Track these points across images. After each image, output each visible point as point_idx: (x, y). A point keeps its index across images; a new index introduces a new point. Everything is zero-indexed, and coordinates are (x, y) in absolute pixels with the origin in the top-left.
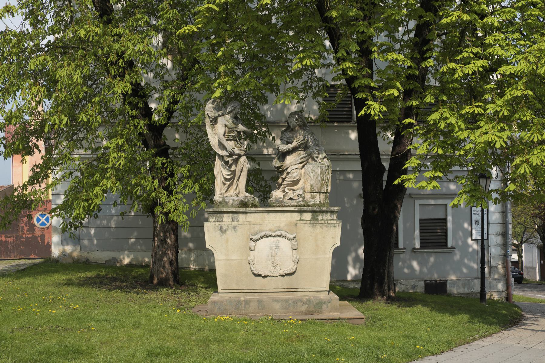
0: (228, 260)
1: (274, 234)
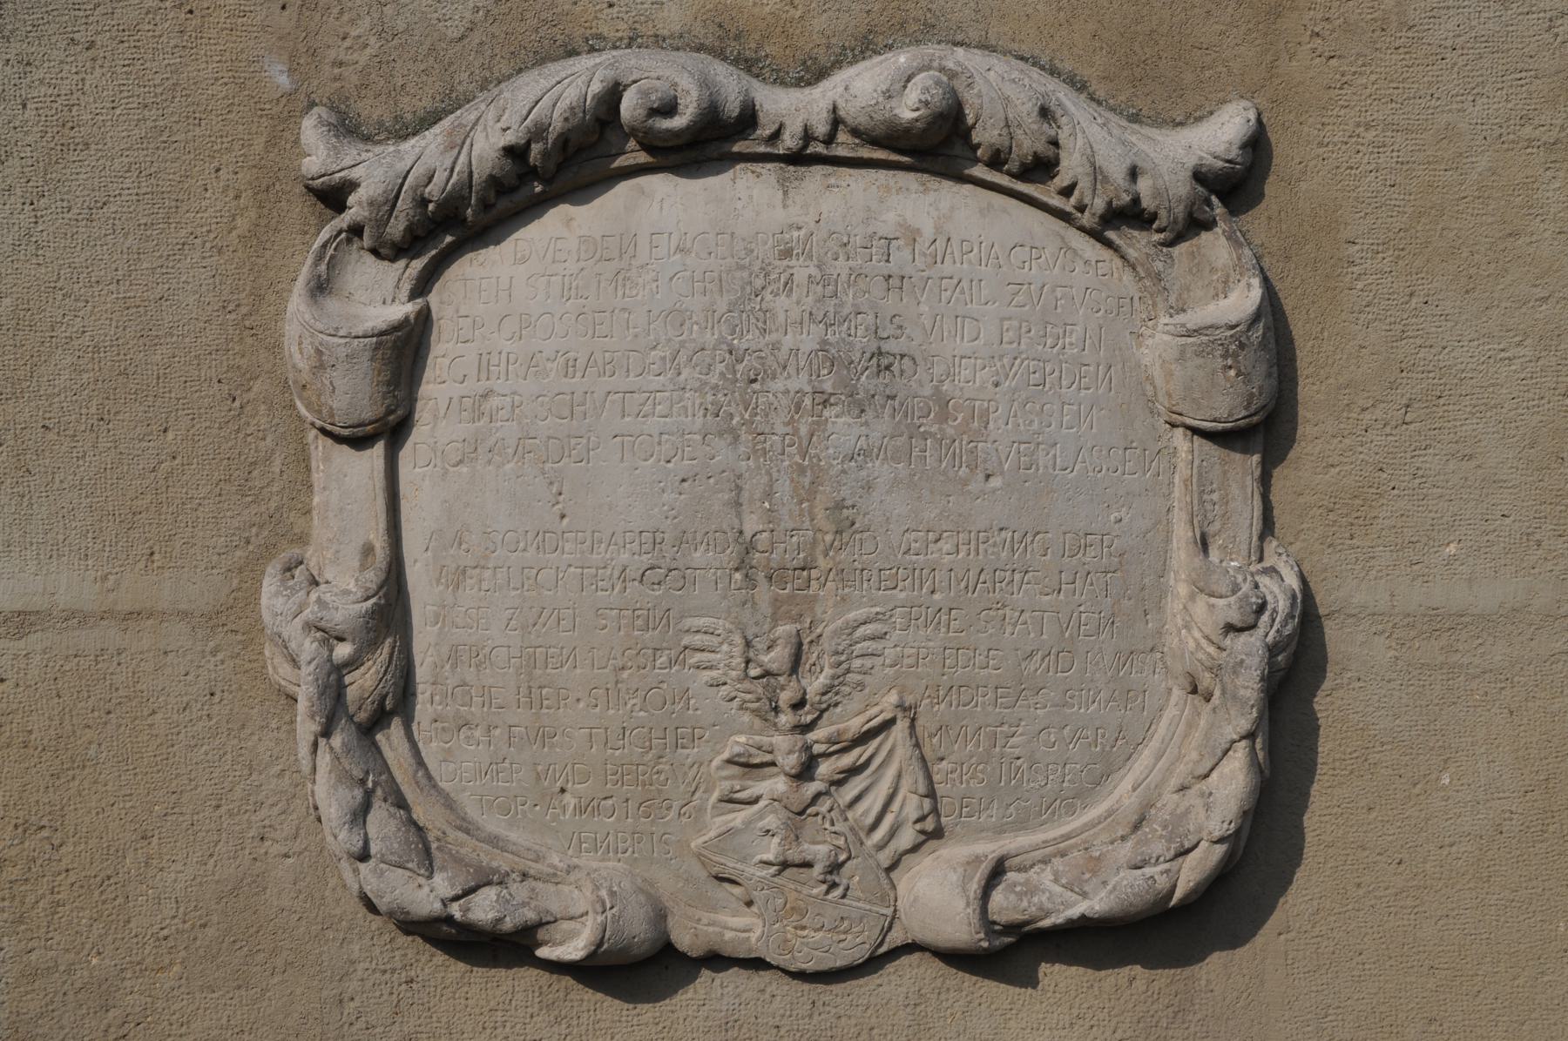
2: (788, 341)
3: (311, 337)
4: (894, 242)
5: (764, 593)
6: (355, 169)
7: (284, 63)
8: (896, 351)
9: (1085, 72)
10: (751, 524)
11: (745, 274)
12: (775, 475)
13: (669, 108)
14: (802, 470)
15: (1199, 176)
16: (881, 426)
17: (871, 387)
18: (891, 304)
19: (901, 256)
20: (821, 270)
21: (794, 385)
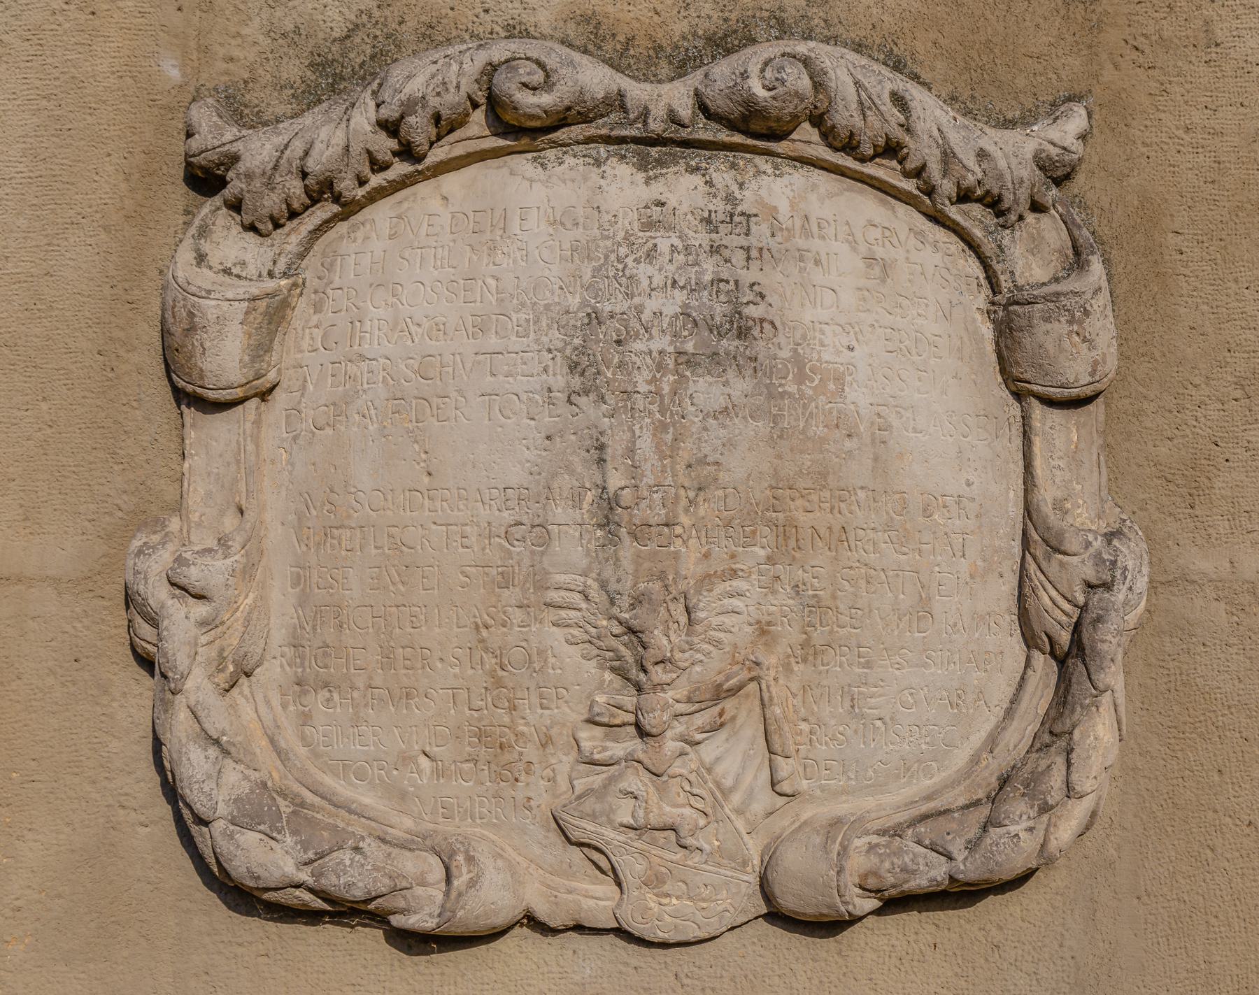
2: (651, 305)
3: (184, 300)
4: (753, 219)
5: (628, 549)
6: (235, 144)
7: (176, 58)
8: (755, 315)
10: (616, 481)
11: (609, 243)
12: (638, 433)
14: (663, 427)
17: (731, 348)
20: (682, 241)
21: (655, 346)
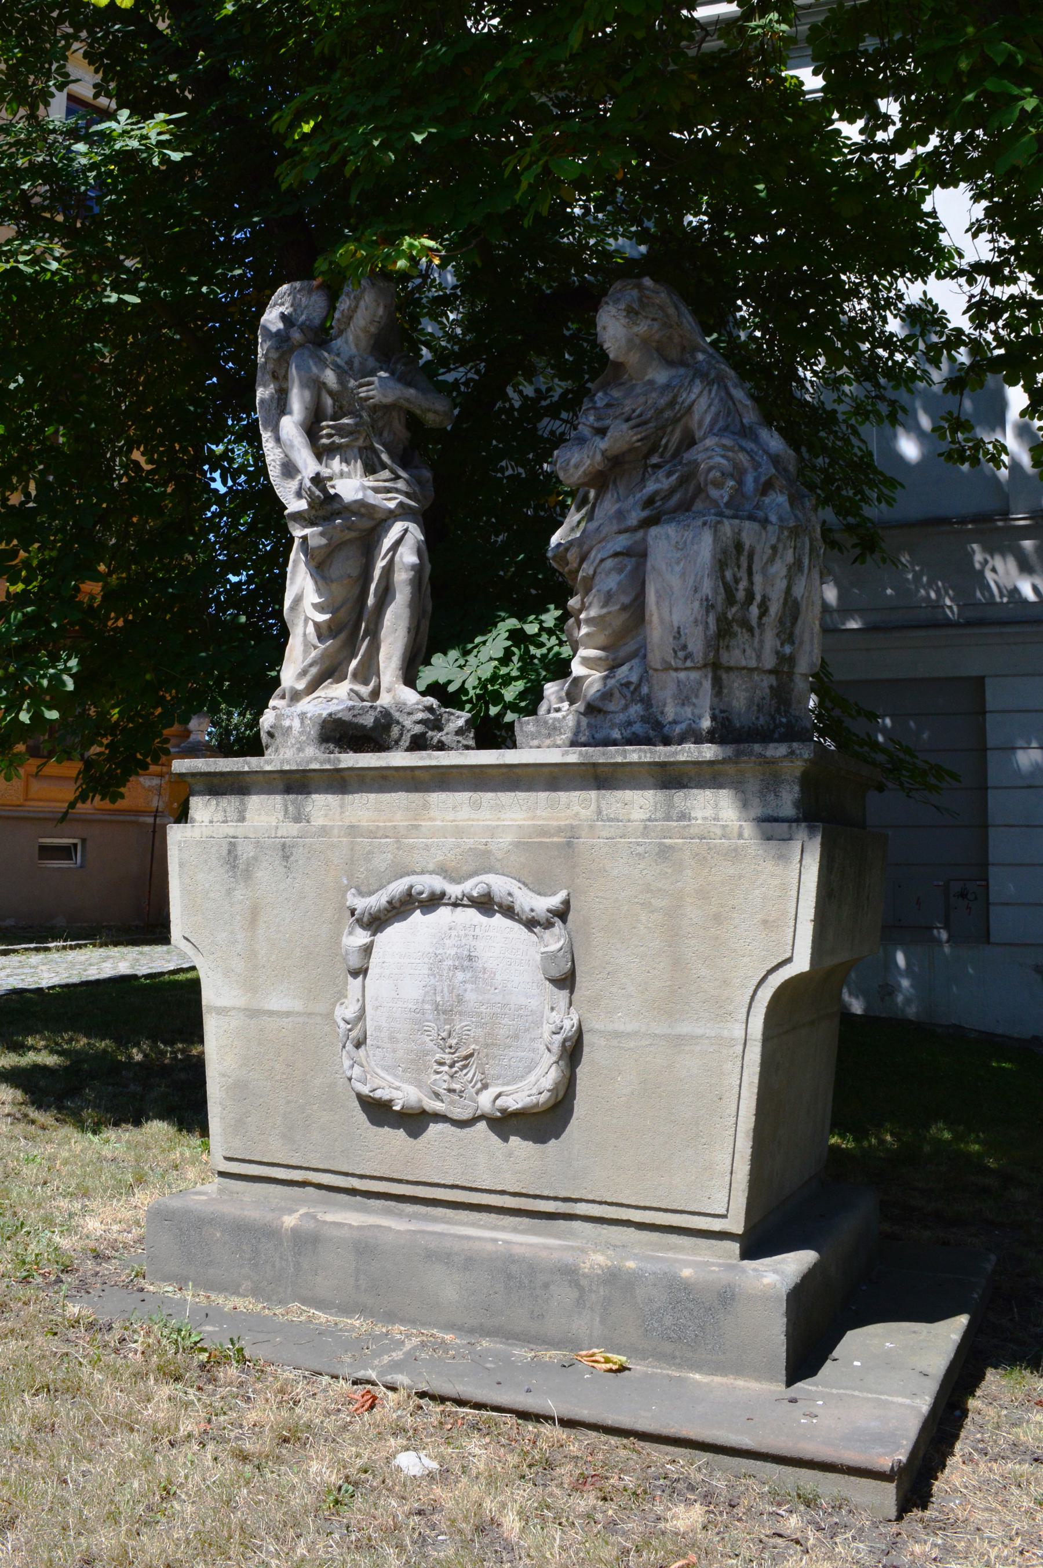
0: (253, 1013)
1: (454, 890)
9: (527, 881)
10: (438, 999)
13: (422, 893)
15: (549, 911)
16: (469, 975)
18: (473, 943)
19: (478, 929)
